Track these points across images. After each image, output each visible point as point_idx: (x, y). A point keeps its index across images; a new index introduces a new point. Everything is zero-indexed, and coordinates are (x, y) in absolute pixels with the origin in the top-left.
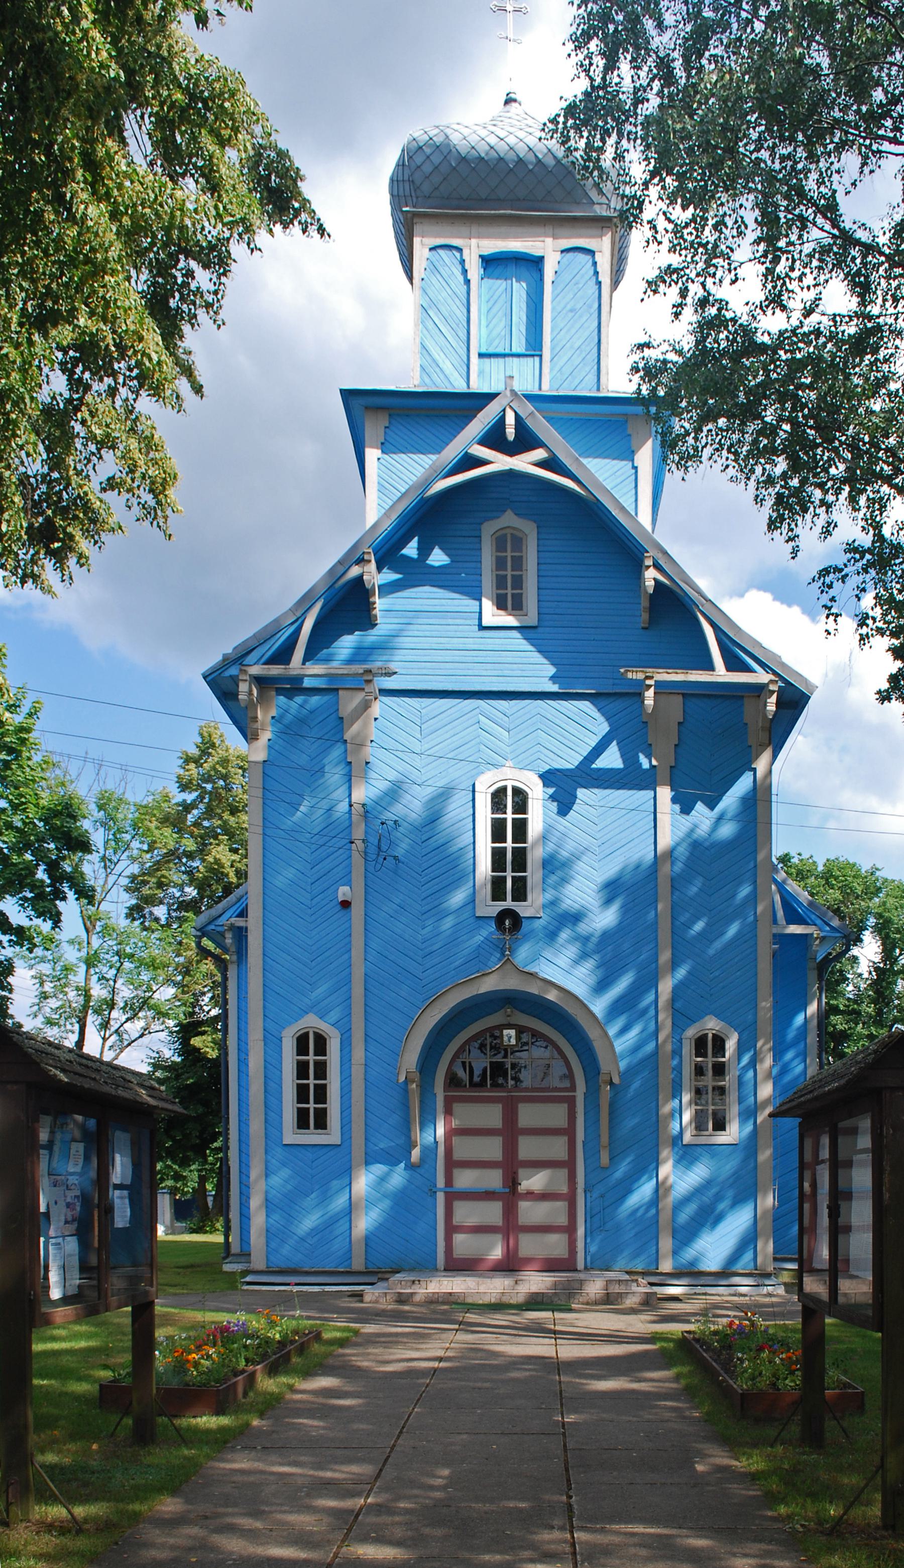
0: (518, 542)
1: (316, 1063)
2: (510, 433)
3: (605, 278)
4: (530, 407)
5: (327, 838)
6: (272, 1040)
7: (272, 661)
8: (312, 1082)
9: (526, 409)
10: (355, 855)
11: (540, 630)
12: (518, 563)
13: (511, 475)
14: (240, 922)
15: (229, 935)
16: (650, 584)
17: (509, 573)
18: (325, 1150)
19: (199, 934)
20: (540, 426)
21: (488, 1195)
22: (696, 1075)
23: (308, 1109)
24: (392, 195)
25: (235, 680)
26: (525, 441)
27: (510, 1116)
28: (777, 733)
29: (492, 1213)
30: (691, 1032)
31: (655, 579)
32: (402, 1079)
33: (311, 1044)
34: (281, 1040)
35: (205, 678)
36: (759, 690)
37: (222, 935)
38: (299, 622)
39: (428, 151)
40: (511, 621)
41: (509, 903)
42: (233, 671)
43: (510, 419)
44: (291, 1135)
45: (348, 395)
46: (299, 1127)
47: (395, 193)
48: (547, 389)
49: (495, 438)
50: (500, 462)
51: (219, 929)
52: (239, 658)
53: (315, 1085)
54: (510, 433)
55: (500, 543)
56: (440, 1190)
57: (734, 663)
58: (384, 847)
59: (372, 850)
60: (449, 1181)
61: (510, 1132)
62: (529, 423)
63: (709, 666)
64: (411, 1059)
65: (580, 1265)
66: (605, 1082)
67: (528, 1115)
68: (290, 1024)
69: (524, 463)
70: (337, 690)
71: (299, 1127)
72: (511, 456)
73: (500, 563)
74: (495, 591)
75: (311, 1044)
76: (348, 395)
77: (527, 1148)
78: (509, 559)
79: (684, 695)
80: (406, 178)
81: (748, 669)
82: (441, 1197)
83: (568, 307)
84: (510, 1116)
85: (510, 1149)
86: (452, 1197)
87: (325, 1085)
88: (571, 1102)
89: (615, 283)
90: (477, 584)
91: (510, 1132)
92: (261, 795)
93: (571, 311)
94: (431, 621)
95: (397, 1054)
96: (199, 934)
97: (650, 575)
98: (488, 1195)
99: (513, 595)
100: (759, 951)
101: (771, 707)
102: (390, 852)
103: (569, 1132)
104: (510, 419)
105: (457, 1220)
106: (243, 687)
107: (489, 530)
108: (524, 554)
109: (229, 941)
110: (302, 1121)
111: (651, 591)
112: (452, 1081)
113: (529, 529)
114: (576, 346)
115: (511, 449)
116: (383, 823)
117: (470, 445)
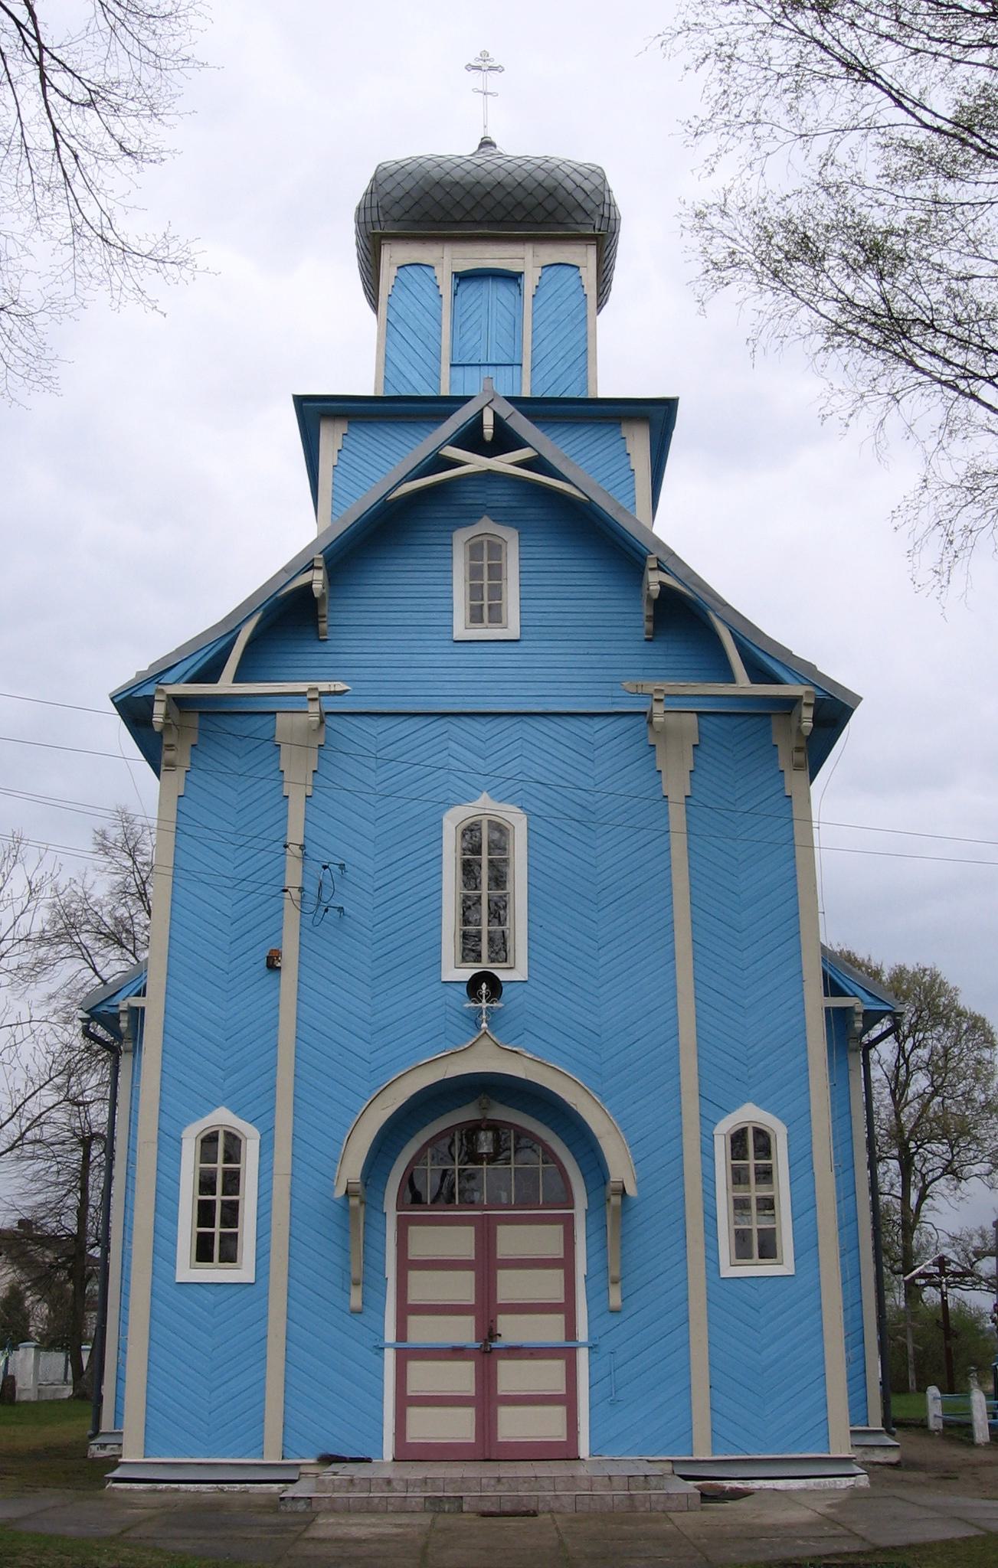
0: (496, 549)
1: (226, 1172)
2: (488, 432)
3: (592, 291)
4: (511, 408)
5: (256, 885)
6: (169, 1144)
7: (196, 679)
8: (218, 1197)
9: (506, 410)
10: (287, 903)
11: (522, 644)
12: (496, 572)
13: (490, 475)
14: (136, 1002)
15: (124, 1018)
16: (655, 588)
17: (486, 582)
18: (234, 1289)
19: (86, 1016)
20: (520, 424)
21: (456, 1353)
22: (734, 1183)
23: (213, 1234)
24: (358, 223)
25: (150, 701)
26: (506, 440)
27: (486, 1241)
28: (815, 751)
29: (461, 1377)
30: (726, 1126)
31: (660, 583)
32: (340, 1192)
33: (221, 1147)
34: (180, 1142)
35: (112, 699)
36: (790, 704)
37: (116, 1018)
38: (234, 634)
39: (398, 178)
40: (512, 310)
41: (485, 965)
42: (149, 690)
43: (488, 420)
44: (188, 1270)
45: (302, 402)
46: (199, 1260)
47: (362, 220)
48: (526, 393)
49: (471, 438)
50: (476, 463)
51: (113, 1010)
52: (158, 674)
53: (223, 1202)
54: (488, 432)
55: (475, 551)
56: (390, 1345)
57: (759, 673)
58: (325, 897)
59: (312, 898)
60: (402, 1333)
61: (486, 1264)
62: (510, 423)
63: (731, 678)
64: (352, 1168)
65: (584, 1451)
66: (615, 1193)
67: (511, 1240)
68: (195, 1120)
69: (502, 463)
70: (274, 713)
71: (199, 1260)
72: (489, 457)
73: (475, 573)
74: (468, 602)
75: (221, 1147)
76: (302, 402)
77: (510, 1286)
78: (486, 588)
79: (698, 713)
80: (374, 204)
81: (776, 680)
82: (390, 1356)
83: (551, 319)
84: (486, 1241)
85: (486, 1287)
86: (405, 1356)
87: (237, 1203)
88: (568, 1222)
89: (600, 306)
90: (446, 622)
91: (486, 1264)
92: (174, 819)
93: (553, 322)
94: (391, 636)
95: (338, 1160)
96: (86, 1016)
97: (654, 580)
98: (456, 1353)
99: (490, 606)
100: (808, 1020)
101: (808, 724)
102: (333, 903)
103: (566, 1264)
104: (488, 420)
105: (414, 1297)
106: (159, 709)
107: (461, 539)
108: (503, 562)
109: (123, 1025)
110: (204, 1252)
111: (656, 596)
112: (412, 1195)
113: (511, 538)
114: (561, 355)
115: (490, 450)
116: (325, 867)
117: (441, 446)
